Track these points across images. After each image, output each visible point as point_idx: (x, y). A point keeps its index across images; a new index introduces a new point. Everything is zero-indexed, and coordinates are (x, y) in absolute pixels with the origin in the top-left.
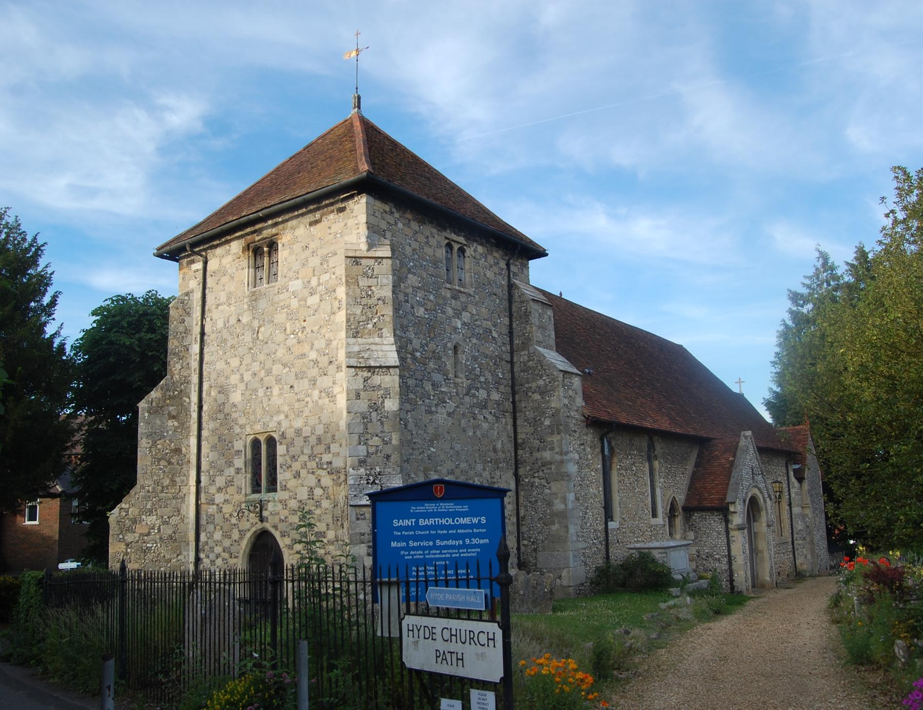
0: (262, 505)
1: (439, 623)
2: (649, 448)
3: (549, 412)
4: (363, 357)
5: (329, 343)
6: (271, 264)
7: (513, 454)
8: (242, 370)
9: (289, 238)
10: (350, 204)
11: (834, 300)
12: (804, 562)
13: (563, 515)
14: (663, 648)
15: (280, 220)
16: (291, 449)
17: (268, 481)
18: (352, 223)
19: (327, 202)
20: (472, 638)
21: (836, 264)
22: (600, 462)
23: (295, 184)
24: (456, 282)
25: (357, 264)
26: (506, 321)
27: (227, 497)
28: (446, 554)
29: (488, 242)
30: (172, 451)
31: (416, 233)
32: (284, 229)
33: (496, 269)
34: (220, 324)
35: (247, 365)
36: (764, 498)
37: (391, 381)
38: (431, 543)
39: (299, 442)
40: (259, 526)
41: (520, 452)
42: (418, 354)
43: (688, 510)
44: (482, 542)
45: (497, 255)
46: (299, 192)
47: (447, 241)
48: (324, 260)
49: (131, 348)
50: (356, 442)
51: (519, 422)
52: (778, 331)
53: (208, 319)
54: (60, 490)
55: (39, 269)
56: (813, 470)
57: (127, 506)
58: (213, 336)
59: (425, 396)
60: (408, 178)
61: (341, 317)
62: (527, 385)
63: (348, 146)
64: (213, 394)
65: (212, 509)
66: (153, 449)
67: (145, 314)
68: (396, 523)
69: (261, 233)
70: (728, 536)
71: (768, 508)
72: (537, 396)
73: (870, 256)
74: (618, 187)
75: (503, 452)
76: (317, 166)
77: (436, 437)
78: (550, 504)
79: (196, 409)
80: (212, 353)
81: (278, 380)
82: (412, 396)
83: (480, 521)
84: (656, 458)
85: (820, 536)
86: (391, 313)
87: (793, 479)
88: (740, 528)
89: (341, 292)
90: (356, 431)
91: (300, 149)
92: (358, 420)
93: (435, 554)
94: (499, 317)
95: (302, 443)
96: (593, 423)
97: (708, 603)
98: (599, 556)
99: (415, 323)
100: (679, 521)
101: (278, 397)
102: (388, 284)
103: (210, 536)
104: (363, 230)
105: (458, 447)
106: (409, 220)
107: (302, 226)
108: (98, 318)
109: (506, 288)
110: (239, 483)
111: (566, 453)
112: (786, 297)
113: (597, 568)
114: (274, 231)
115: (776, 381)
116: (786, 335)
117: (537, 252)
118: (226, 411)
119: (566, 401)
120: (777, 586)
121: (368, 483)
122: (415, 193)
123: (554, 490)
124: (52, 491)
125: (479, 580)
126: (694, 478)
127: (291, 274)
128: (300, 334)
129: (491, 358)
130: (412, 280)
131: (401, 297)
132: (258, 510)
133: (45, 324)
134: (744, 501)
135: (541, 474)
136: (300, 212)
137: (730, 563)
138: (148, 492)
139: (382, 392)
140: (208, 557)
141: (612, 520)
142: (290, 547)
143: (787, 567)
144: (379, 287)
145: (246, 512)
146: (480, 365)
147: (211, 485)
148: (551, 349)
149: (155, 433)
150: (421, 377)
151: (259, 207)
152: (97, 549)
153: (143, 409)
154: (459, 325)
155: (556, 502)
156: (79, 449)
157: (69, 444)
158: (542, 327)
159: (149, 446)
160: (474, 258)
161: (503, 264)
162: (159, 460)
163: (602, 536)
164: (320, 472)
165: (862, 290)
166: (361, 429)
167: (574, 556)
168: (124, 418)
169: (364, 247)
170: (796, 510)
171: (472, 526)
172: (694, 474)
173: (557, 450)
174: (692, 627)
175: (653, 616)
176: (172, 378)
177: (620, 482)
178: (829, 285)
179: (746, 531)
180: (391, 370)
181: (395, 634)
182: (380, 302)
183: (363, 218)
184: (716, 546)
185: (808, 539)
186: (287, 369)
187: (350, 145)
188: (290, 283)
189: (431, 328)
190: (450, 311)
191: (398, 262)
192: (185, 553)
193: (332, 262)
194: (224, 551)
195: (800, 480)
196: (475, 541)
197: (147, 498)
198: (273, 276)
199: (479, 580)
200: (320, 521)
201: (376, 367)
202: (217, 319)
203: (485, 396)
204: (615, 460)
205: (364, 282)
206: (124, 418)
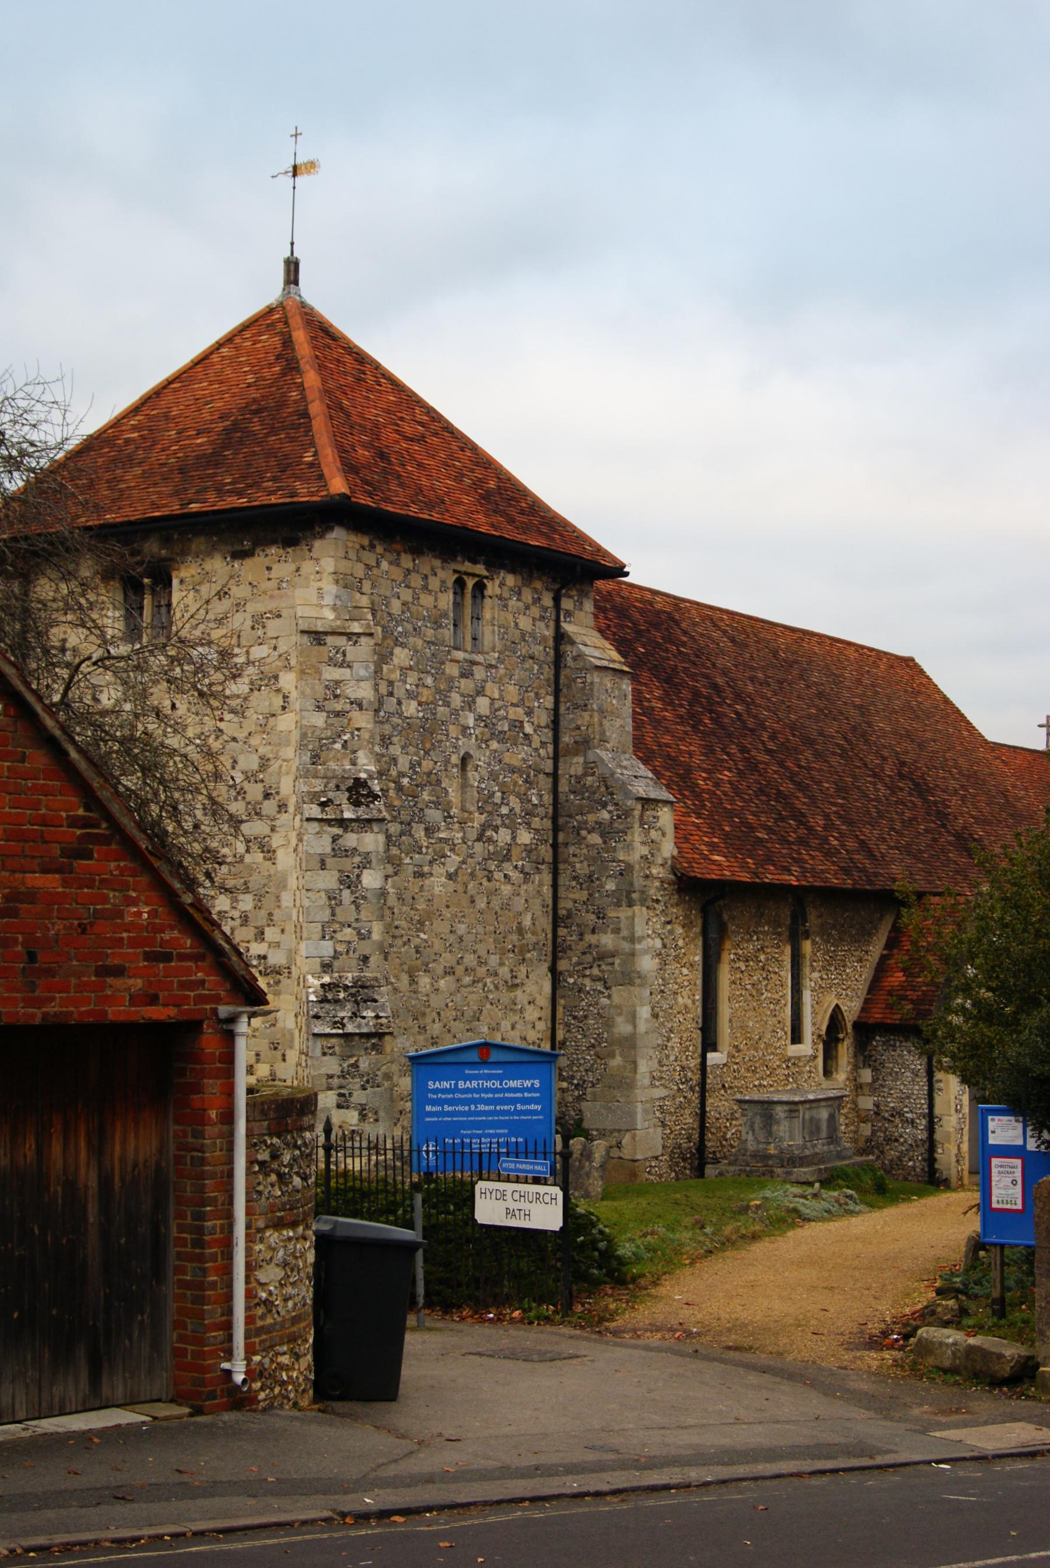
5: (264, 763)
7: (550, 936)
13: (629, 1043)
20: (538, 1197)
22: (699, 951)
26: (549, 701)
33: (535, 611)
38: (467, 1108)
41: (562, 932)
42: (405, 781)
43: (864, 1031)
45: (538, 585)
47: (456, 576)
48: (259, 621)
51: (562, 880)
62: (579, 817)
72: (595, 839)
75: (534, 933)
82: (395, 851)
83: (532, 1084)
94: (537, 696)
100: (845, 1051)
106: (398, 554)
109: (551, 643)
125: (536, 1153)
128: (211, 740)
130: (401, 656)
137: (931, 1129)
141: (715, 1050)
150: (409, 818)
155: (619, 1020)
160: (500, 598)
161: (548, 601)
163: (696, 1078)
167: (645, 1111)
171: (522, 1090)
172: (883, 959)
173: (625, 933)
177: (734, 982)
184: (908, 1098)
190: (456, 700)
203: (508, 839)
204: (728, 945)
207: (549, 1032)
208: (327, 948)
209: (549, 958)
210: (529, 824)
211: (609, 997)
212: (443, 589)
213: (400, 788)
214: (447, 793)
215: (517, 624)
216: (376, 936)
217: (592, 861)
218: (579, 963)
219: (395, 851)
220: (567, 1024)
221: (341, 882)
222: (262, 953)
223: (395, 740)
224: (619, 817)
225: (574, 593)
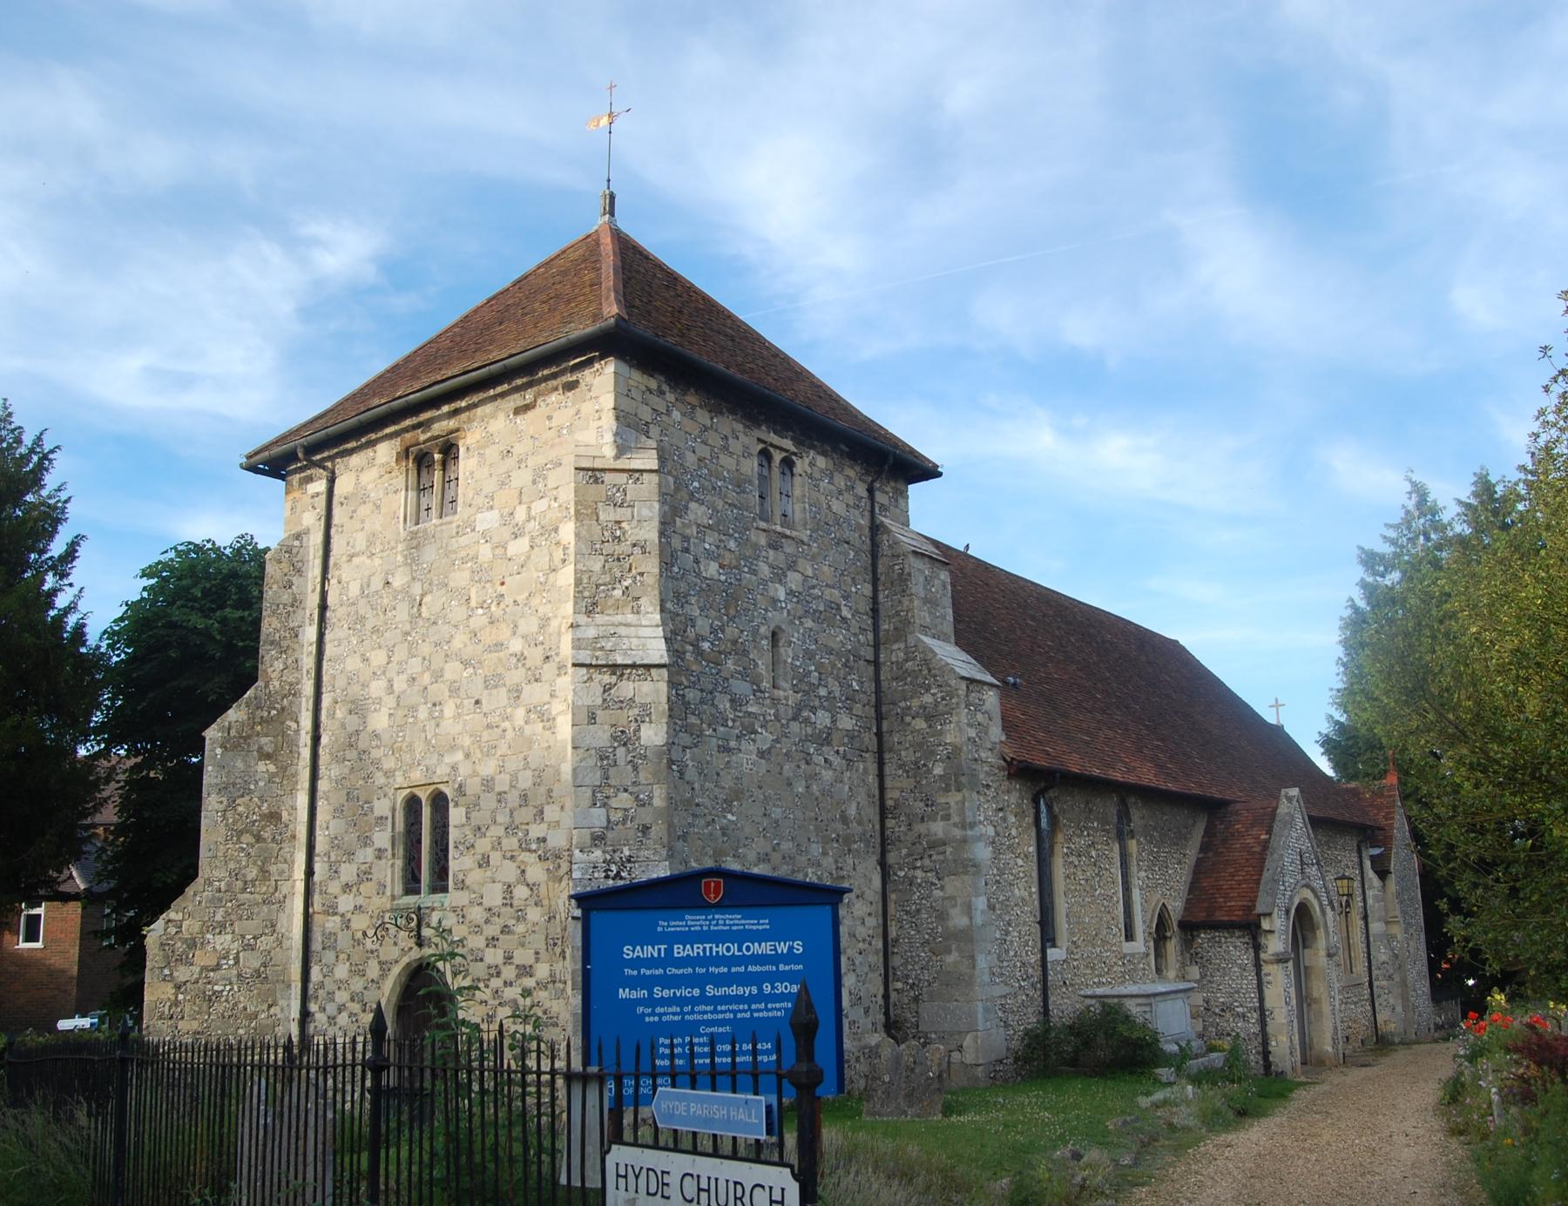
0: (420, 915)
1: (677, 1164)
2: (1120, 817)
3: (942, 752)
4: (602, 649)
5: (545, 622)
6: (446, 482)
7: (877, 827)
8: (391, 673)
9: (478, 437)
10: (587, 375)
11: (1436, 564)
12: (1390, 1019)
13: (965, 937)
14: (1143, 1185)
15: (463, 404)
16: (474, 815)
17: (432, 869)
18: (587, 413)
19: (546, 372)
21: (1440, 504)
22: (1033, 842)
23: (492, 342)
24: (778, 518)
25: (596, 481)
26: (867, 589)
27: (360, 901)
28: (725, 1012)
29: (834, 449)
30: (263, 817)
31: (706, 429)
32: (470, 421)
34: (354, 590)
35: (400, 663)
36: (1321, 905)
37: (654, 691)
38: (696, 992)
39: (489, 802)
40: (416, 954)
41: (890, 823)
42: (706, 645)
43: (1189, 928)
45: (851, 473)
47: (761, 446)
48: (539, 475)
49: (206, 634)
50: (588, 802)
51: (887, 770)
52: (1342, 619)
53: (333, 582)
54: (82, 887)
55: (44, 493)
56: (1404, 859)
57: (180, 916)
58: (341, 611)
59: (719, 720)
60: (693, 334)
61: (566, 577)
62: (902, 704)
63: (588, 276)
64: (339, 714)
65: (333, 923)
66: (229, 814)
67: (234, 575)
68: (629, 952)
69: (429, 428)
70: (1258, 974)
72: (920, 724)
73: (1499, 489)
74: (1070, 382)
75: (860, 823)
77: (737, 794)
78: (942, 916)
79: (309, 742)
80: (340, 641)
81: (454, 690)
82: (693, 720)
83: (791, 948)
84: (1132, 834)
85: (1417, 972)
86: (656, 570)
87: (1370, 874)
88: (1280, 960)
89: (568, 532)
90: (587, 781)
92: (591, 762)
93: (704, 1012)
95: (494, 804)
96: (1019, 771)
97: (1225, 1096)
99: (702, 589)
100: (1172, 946)
101: (454, 721)
102: (651, 519)
103: (328, 972)
104: (609, 422)
105: (777, 813)
106: (693, 407)
108: (153, 581)
111: (972, 825)
112: (1355, 560)
113: (1027, 1033)
114: (452, 424)
115: (1340, 705)
116: (1356, 623)
117: (924, 471)
118: (362, 745)
119: (972, 733)
120: (1346, 1061)
121: (607, 877)
122: (705, 359)
123: (950, 890)
124: (62, 888)
126: (1199, 871)
127: (480, 500)
128: (493, 608)
129: (839, 655)
130: (697, 512)
131: (676, 542)
132: (413, 924)
133: (54, 592)
134: (1288, 912)
135: (927, 862)
136: (499, 389)
137: (1263, 1022)
138: (219, 890)
139: (636, 711)
140: (323, 1009)
141: (1054, 946)
143: (1362, 1028)
144: (635, 523)
145: (393, 929)
146: (820, 668)
147: (331, 878)
148: (946, 640)
149: (234, 784)
150: (711, 687)
151: (426, 381)
152: (126, 996)
154: (781, 594)
159: (222, 807)
160: (811, 477)
161: (861, 490)
162: (240, 833)
163: (1036, 974)
164: (525, 856)
166: (596, 777)
167: (986, 1010)
169: (609, 451)
170: (1376, 927)
171: (776, 959)
172: (1199, 862)
173: (955, 819)
174: (1196, 1143)
175: (1125, 1123)
176: (267, 686)
178: (1428, 539)
179: (1290, 964)
180: (653, 671)
181: (593, 1182)
182: (637, 550)
183: (608, 401)
185: (1397, 978)
186: (471, 670)
188: (479, 516)
189: (730, 599)
190: (765, 570)
191: (671, 479)
192: (282, 1003)
193: (553, 478)
194: (352, 1000)
195: (1383, 874)
196: (781, 988)
197: (216, 902)
198: (448, 504)
199: (755, 1077)
200: (523, 945)
201: (626, 666)
202: (349, 581)
203: (828, 722)
204: (1060, 838)
205: (607, 515)
207: (880, 930)
208: (598, 817)
209: (878, 850)
210: (850, 709)
211: (942, 888)
212: (747, 454)
213: (699, 653)
214: (756, 665)
215: (829, 507)
216: (658, 802)
218: (908, 855)
220: (900, 921)
221: (615, 739)
225: (888, 489)
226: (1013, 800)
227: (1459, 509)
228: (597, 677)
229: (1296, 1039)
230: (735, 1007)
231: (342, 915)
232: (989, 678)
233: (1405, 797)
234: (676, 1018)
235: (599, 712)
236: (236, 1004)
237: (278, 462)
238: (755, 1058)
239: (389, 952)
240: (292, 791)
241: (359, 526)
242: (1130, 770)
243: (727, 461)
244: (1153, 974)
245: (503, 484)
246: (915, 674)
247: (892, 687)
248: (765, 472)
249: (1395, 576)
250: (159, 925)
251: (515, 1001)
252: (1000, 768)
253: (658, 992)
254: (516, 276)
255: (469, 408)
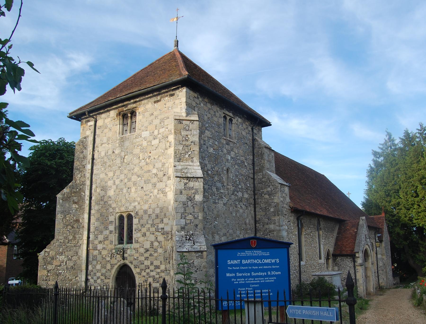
0: (124, 251)
5: (164, 164)
6: (132, 123)
7: (254, 226)
9: (142, 109)
10: (177, 92)
11: (393, 155)
12: (383, 282)
15: (138, 100)
16: (141, 221)
17: (127, 238)
18: (178, 102)
19: (164, 91)
22: (297, 231)
23: (145, 82)
24: (228, 136)
25: (181, 123)
26: (251, 157)
27: (104, 246)
29: (243, 117)
30: (74, 221)
31: (209, 109)
32: (140, 105)
34: (103, 154)
35: (117, 176)
36: (370, 250)
37: (199, 185)
38: (249, 274)
39: (146, 217)
40: (122, 262)
41: (257, 225)
42: (210, 172)
43: (335, 256)
44: (277, 273)
45: (247, 124)
46: (148, 86)
47: (224, 115)
48: (162, 121)
50: (179, 218)
52: (367, 170)
57: (49, 250)
58: (99, 160)
59: (213, 194)
62: (261, 191)
63: (174, 64)
64: (98, 191)
65: (96, 253)
66: (64, 220)
67: (58, 150)
68: (229, 262)
70: (355, 269)
71: (372, 254)
72: (267, 196)
73: (411, 135)
75: (249, 225)
76: (158, 73)
77: (218, 216)
79: (88, 199)
81: (135, 184)
82: (206, 194)
83: (276, 261)
88: (361, 265)
89: (171, 138)
90: (180, 211)
91: (146, 65)
92: (181, 206)
93: (251, 281)
95: (147, 218)
98: (296, 279)
100: (330, 261)
104: (184, 106)
105: (228, 221)
107: (150, 103)
109: (251, 140)
110: (111, 239)
111: (282, 226)
114: (134, 105)
115: (366, 194)
117: (268, 124)
118: (105, 200)
119: (282, 199)
121: (186, 240)
126: (337, 240)
127: (143, 128)
128: (147, 160)
130: (207, 133)
134: (363, 252)
136: (149, 96)
138: (61, 242)
139: (194, 191)
140: (92, 278)
142: (140, 274)
144: (192, 136)
146: (239, 179)
147: (95, 239)
148: (273, 173)
150: (211, 184)
153: (59, 198)
156: (20, 220)
157: (16, 217)
158: (269, 161)
159: (62, 218)
162: (67, 226)
163: (298, 268)
164: (157, 233)
165: (407, 151)
166: (182, 210)
168: (44, 204)
169: (184, 114)
170: (379, 256)
171: (271, 264)
172: (337, 238)
173: (277, 224)
178: (391, 148)
180: (199, 179)
182: (193, 144)
183: (184, 100)
185: (385, 271)
187: (175, 63)
189: (216, 159)
190: (225, 151)
191: (201, 123)
193: (166, 122)
194: (102, 275)
196: (273, 273)
197: (60, 246)
198: (133, 129)
200: (156, 260)
203: (241, 195)
204: (303, 230)
205: (184, 133)
206: (44, 204)
208: (183, 222)
209: (254, 233)
212: (220, 117)
216: (200, 218)
217: (266, 203)
218: (263, 234)
219: (206, 194)
222: (162, 227)
223: (206, 159)
224: (274, 189)
226: (292, 219)
227: (400, 140)
228: (182, 180)
229: (365, 287)
230: (260, 279)
231: (99, 250)
232: (286, 184)
233: (386, 220)
234: (243, 282)
235: (183, 191)
236: (66, 276)
237: (78, 116)
238: (261, 294)
239: (114, 261)
240: (83, 213)
241: (104, 135)
242: (321, 211)
243: (215, 119)
244: (326, 269)
245: (150, 123)
246: (265, 182)
247: (258, 186)
248: (225, 123)
249: (382, 158)
250: (43, 253)
251: (154, 276)
252: (289, 210)
253: (238, 274)
254: (150, 63)
255: (139, 101)
